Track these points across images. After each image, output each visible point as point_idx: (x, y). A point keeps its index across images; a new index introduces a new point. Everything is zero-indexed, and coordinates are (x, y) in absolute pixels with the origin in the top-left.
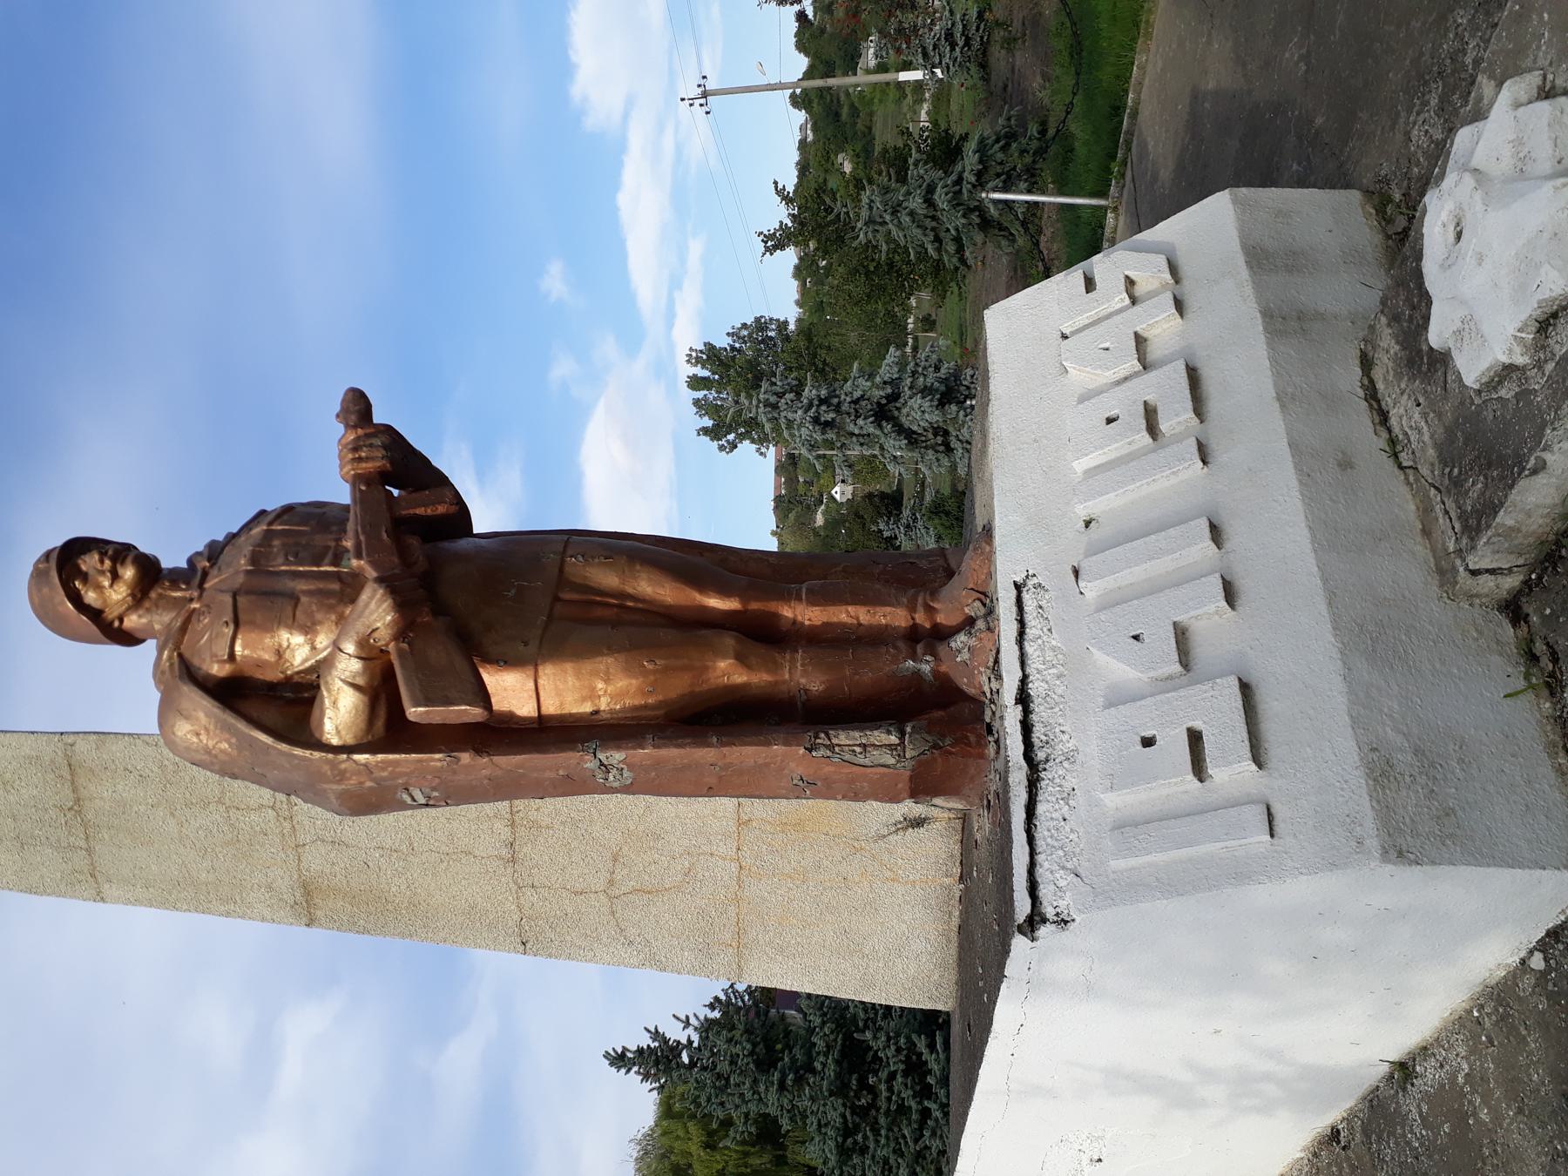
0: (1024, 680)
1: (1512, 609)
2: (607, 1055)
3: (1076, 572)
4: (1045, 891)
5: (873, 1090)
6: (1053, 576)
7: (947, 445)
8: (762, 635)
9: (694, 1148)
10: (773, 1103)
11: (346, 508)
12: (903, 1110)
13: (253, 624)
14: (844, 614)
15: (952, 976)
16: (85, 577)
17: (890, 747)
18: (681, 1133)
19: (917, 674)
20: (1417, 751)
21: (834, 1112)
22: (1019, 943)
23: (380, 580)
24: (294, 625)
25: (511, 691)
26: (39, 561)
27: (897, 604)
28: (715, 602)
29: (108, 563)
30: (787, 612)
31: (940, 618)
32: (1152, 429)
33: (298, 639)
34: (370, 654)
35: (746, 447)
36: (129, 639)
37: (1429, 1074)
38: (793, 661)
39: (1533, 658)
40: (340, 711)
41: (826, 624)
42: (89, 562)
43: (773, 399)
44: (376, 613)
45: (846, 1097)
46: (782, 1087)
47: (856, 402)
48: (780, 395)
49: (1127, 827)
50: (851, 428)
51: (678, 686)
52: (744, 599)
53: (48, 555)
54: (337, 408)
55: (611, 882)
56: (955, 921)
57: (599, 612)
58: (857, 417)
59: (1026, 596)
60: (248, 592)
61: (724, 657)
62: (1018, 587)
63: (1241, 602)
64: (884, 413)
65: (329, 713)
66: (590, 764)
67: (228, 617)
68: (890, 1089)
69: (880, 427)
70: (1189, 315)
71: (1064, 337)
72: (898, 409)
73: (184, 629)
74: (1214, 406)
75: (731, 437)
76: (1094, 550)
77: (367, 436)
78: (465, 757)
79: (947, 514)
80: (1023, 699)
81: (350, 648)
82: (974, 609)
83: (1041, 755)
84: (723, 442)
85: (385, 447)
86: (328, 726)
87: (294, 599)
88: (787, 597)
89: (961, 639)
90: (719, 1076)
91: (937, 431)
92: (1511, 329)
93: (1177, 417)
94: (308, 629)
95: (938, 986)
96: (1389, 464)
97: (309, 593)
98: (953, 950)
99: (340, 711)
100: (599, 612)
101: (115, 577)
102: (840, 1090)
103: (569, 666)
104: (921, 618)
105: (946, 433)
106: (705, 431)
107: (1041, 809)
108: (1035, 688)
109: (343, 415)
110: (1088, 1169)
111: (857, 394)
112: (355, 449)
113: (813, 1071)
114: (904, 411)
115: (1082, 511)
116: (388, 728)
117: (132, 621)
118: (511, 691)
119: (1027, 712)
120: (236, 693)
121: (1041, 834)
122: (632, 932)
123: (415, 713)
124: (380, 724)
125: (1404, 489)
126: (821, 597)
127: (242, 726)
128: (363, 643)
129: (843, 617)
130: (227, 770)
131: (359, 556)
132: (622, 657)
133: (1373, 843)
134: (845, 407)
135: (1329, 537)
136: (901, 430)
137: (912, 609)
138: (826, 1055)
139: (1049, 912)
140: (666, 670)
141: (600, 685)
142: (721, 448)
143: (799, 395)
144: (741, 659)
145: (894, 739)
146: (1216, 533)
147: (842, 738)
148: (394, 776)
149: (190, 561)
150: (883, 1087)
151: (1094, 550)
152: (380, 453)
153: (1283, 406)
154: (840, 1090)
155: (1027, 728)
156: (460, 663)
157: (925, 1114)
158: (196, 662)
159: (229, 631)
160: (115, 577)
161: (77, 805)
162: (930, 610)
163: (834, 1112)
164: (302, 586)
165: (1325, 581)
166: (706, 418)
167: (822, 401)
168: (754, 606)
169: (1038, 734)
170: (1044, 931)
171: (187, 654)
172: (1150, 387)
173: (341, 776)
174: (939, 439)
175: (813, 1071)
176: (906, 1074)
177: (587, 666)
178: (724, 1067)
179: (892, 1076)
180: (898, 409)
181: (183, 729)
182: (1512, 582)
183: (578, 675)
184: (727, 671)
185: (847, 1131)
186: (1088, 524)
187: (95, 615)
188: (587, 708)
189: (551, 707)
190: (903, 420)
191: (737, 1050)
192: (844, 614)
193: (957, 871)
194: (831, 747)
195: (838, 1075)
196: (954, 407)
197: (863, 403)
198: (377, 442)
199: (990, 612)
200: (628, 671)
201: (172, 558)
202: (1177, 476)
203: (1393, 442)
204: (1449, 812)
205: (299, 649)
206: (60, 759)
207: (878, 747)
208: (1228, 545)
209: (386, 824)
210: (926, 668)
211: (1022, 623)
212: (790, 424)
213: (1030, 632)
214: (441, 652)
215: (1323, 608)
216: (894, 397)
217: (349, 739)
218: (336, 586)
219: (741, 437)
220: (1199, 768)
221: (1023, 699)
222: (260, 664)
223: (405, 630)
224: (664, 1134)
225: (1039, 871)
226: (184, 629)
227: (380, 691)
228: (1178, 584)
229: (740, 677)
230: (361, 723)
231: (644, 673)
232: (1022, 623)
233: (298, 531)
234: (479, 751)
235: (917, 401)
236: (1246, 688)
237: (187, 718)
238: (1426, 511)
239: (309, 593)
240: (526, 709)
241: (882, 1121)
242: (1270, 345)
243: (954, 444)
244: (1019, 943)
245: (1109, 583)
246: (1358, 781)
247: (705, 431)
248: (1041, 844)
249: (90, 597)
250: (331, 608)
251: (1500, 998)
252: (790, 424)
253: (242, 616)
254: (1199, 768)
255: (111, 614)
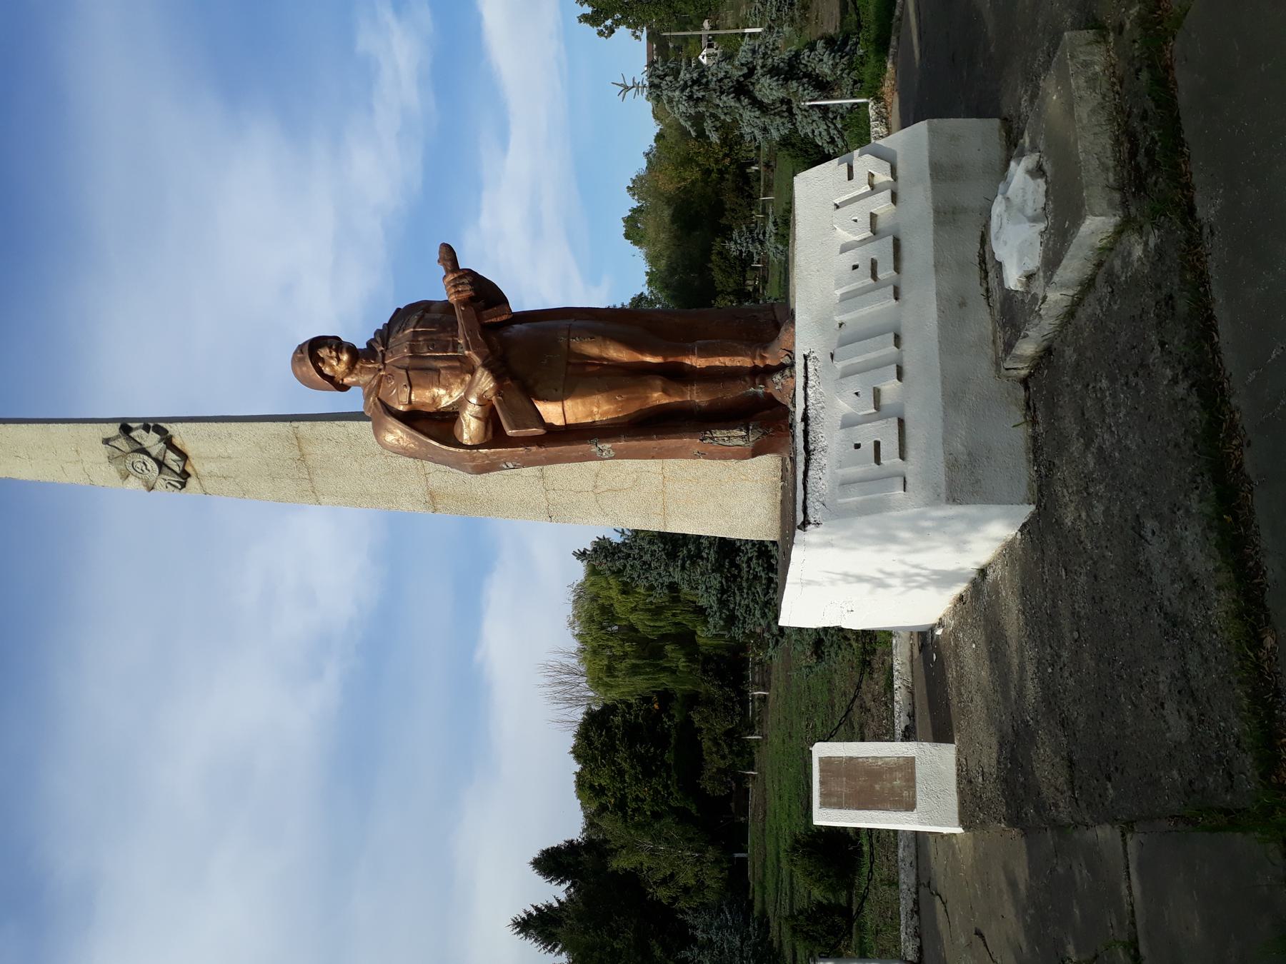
0: (806, 409)
1: (1025, 382)
2: (575, 553)
3: (832, 356)
4: (810, 511)
5: (738, 567)
6: (820, 353)
7: (790, 110)
8: (676, 375)
9: (614, 593)
10: (677, 576)
11: (447, 307)
12: (756, 577)
13: (419, 386)
14: (718, 361)
15: (777, 524)
16: (323, 360)
17: (742, 437)
18: (604, 585)
19: (756, 395)
20: (969, 454)
21: (716, 581)
22: (798, 531)
23: (485, 366)
24: (439, 385)
25: (552, 412)
26: (295, 353)
27: (746, 355)
28: (649, 359)
29: (334, 354)
30: (688, 362)
31: (768, 362)
32: (874, 275)
33: (442, 392)
34: (483, 401)
35: (623, 32)
36: (343, 388)
37: (991, 576)
38: (691, 391)
39: (1028, 407)
40: (470, 427)
41: (708, 367)
42: (324, 353)
43: (657, 81)
44: (485, 382)
45: (722, 572)
46: (683, 568)
47: (720, 80)
48: (662, 78)
49: (845, 484)
50: (717, 101)
51: (634, 407)
52: (664, 357)
53: (301, 348)
54: (438, 257)
55: (595, 487)
56: (779, 498)
57: (589, 369)
58: (722, 93)
59: (809, 363)
60: (415, 369)
61: (656, 391)
62: (806, 357)
63: (906, 377)
64: (742, 90)
65: (465, 430)
66: (594, 449)
67: (406, 382)
68: (749, 566)
69: (739, 100)
70: (899, 204)
71: (837, 207)
72: (753, 84)
73: (379, 385)
74: (906, 265)
75: (609, 22)
76: (843, 343)
77: (460, 277)
78: (534, 449)
79: (793, 146)
80: (805, 418)
81: (473, 400)
82: (786, 360)
83: (812, 447)
84: (602, 28)
85: (470, 284)
86: (466, 436)
87: (437, 371)
88: (688, 352)
89: (777, 377)
90: (645, 563)
91: (782, 101)
92: (1017, 277)
93: (886, 272)
94: (447, 387)
95: (770, 529)
96: (984, 302)
97: (445, 368)
98: (778, 513)
99: (470, 427)
100: (589, 369)
101: (339, 360)
102: (718, 568)
103: (579, 401)
104: (758, 362)
105: (789, 102)
106: (585, 18)
107: (810, 473)
108: (811, 413)
109: (441, 260)
110: (847, 615)
111: (721, 75)
112: (455, 286)
113: (702, 558)
114: (758, 87)
115: (838, 319)
116: (494, 435)
117: (347, 380)
118: (552, 412)
119: (806, 425)
120: (412, 418)
121: (809, 485)
122: (607, 510)
123: (510, 432)
124: (490, 434)
125: (988, 317)
126: (705, 352)
127: (422, 437)
128: (480, 398)
129: (717, 363)
130: (413, 455)
131: (468, 349)
132: (605, 395)
133: (943, 496)
134: (712, 85)
135: (949, 343)
136: (757, 104)
137: (753, 358)
138: (709, 548)
139: (812, 520)
140: (628, 400)
141: (595, 409)
142: (601, 33)
143: (676, 78)
144: (665, 391)
145: (743, 433)
146: (897, 340)
147: (718, 434)
148: (499, 458)
149: (369, 344)
150: (744, 565)
151: (843, 343)
152: (468, 288)
153: (936, 271)
154: (718, 568)
155: (806, 433)
156: (528, 405)
157: (770, 580)
158: (391, 404)
159: (407, 390)
160: (339, 360)
161: (302, 458)
162: (763, 358)
163: (716, 581)
164: (440, 364)
165: (942, 370)
166: (586, 5)
167: (694, 82)
168: (670, 359)
169: (811, 437)
170: (809, 527)
171: (383, 399)
172: (872, 251)
173: (474, 459)
174: (784, 107)
175: (702, 558)
176: (758, 558)
177: (588, 400)
178: (647, 558)
179: (750, 559)
180: (753, 84)
181: (390, 438)
182: (1024, 372)
183: (584, 405)
184: (658, 398)
185: (723, 591)
186: (841, 325)
187: (330, 379)
188: (590, 420)
189: (571, 420)
190: (757, 94)
191: (655, 547)
192: (718, 361)
193: (780, 474)
194: (712, 438)
195: (716, 560)
196: (795, 84)
197: (726, 81)
198: (465, 281)
199: (792, 365)
200: (609, 402)
201: (361, 345)
202: (880, 306)
203: (987, 290)
204: (978, 481)
205: (445, 397)
206: (291, 435)
207: (736, 437)
208: (903, 347)
209: (494, 476)
210: (760, 391)
211: (806, 377)
212: (670, 100)
213: (811, 383)
214: (517, 400)
215: (939, 384)
216: (752, 71)
217: (476, 442)
218: (458, 364)
219: (617, 23)
220: (877, 460)
221: (805, 418)
222: (424, 404)
223: (499, 391)
224: (592, 585)
225: (808, 502)
226: (379, 385)
227: (490, 418)
228: (877, 367)
229: (665, 400)
230: (482, 434)
231: (617, 402)
232: (806, 377)
233: (415, 315)
234: (540, 446)
235: (766, 81)
236: (901, 422)
237: (392, 433)
238: (995, 332)
239: (445, 368)
240: (559, 422)
241: (744, 584)
242: (936, 232)
243: (795, 110)
244: (798, 531)
245: (847, 362)
246: (942, 468)
247: (585, 18)
248: (809, 490)
249: (327, 370)
250: (457, 376)
251: (1009, 546)
252: (670, 100)
253: (413, 383)
254: (877, 460)
255: (338, 377)
